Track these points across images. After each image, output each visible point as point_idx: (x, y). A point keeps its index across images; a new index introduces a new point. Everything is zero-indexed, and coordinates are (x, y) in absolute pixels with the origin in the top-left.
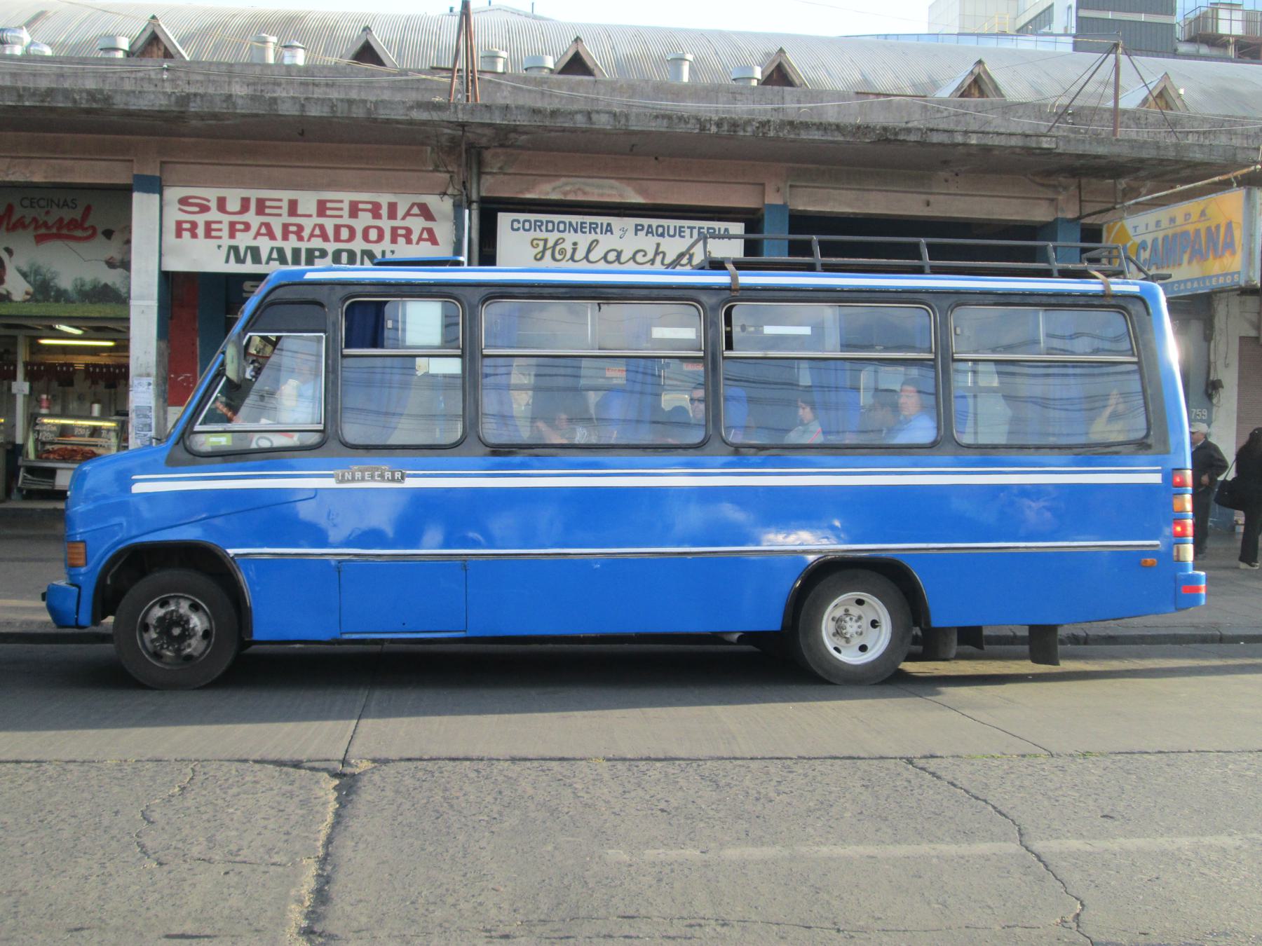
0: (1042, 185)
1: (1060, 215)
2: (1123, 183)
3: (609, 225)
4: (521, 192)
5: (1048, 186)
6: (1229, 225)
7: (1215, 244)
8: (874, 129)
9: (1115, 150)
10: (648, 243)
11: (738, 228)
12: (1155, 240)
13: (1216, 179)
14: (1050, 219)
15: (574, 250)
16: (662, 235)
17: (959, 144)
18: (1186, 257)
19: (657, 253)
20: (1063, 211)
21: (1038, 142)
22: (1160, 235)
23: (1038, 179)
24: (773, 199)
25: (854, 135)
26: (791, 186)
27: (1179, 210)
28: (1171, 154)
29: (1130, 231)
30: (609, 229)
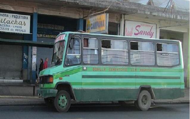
2: (90, 11)
3: (8, 15)
4: (137, 2)
6: (103, 21)
10: (14, 19)
11: (29, 17)
14: (78, 18)
15: (2, 20)
16: (17, 18)
19: (16, 21)
23: (77, 9)
24: (35, 11)
26: (38, 8)
30: (8, 16)
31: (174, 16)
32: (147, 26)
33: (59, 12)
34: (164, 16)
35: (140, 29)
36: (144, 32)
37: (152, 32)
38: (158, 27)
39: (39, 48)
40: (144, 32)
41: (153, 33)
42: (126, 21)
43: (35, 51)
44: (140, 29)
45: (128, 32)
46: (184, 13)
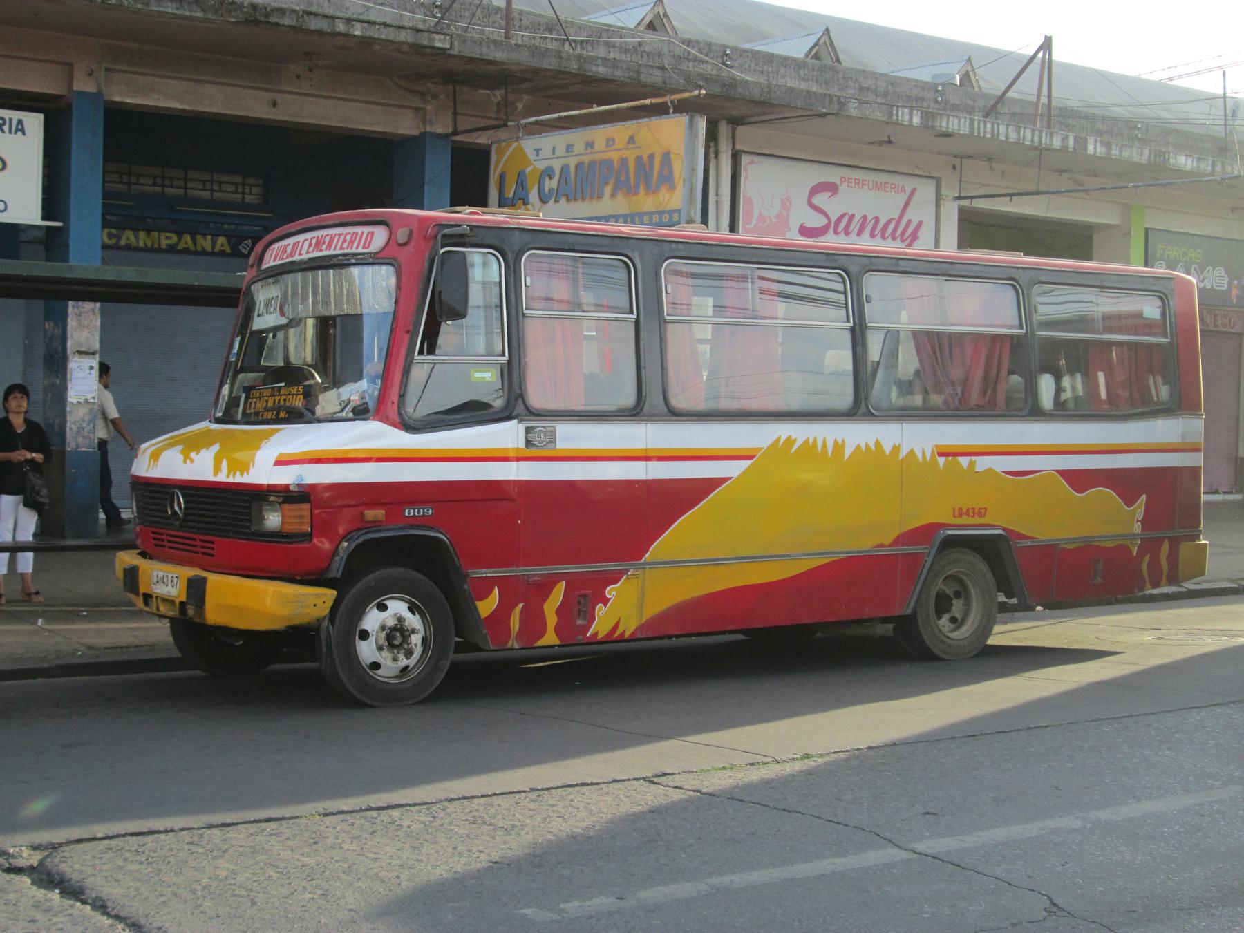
0: (408, 90)
1: (428, 129)
3: (20, 122)
5: (415, 92)
6: (667, 156)
7: (648, 178)
8: (241, 6)
9: (515, 56)
11: (34, 122)
12: (565, 168)
13: (648, 101)
14: (415, 132)
17: (339, 34)
18: (608, 190)
20: (432, 124)
21: (430, 39)
22: (573, 162)
24: (83, 84)
25: (216, 11)
26: (107, 70)
27: (598, 134)
28: (573, 67)
29: (531, 155)
31: (1065, 139)
32: (879, 186)
33: (269, 96)
34: (1007, 136)
35: (834, 206)
36: (865, 217)
37: (909, 222)
38: (949, 192)
39: (109, 306)
40: (865, 217)
41: (920, 224)
42: (745, 160)
43: (85, 333)
44: (834, 206)
45: (762, 218)
46: (1099, 125)
